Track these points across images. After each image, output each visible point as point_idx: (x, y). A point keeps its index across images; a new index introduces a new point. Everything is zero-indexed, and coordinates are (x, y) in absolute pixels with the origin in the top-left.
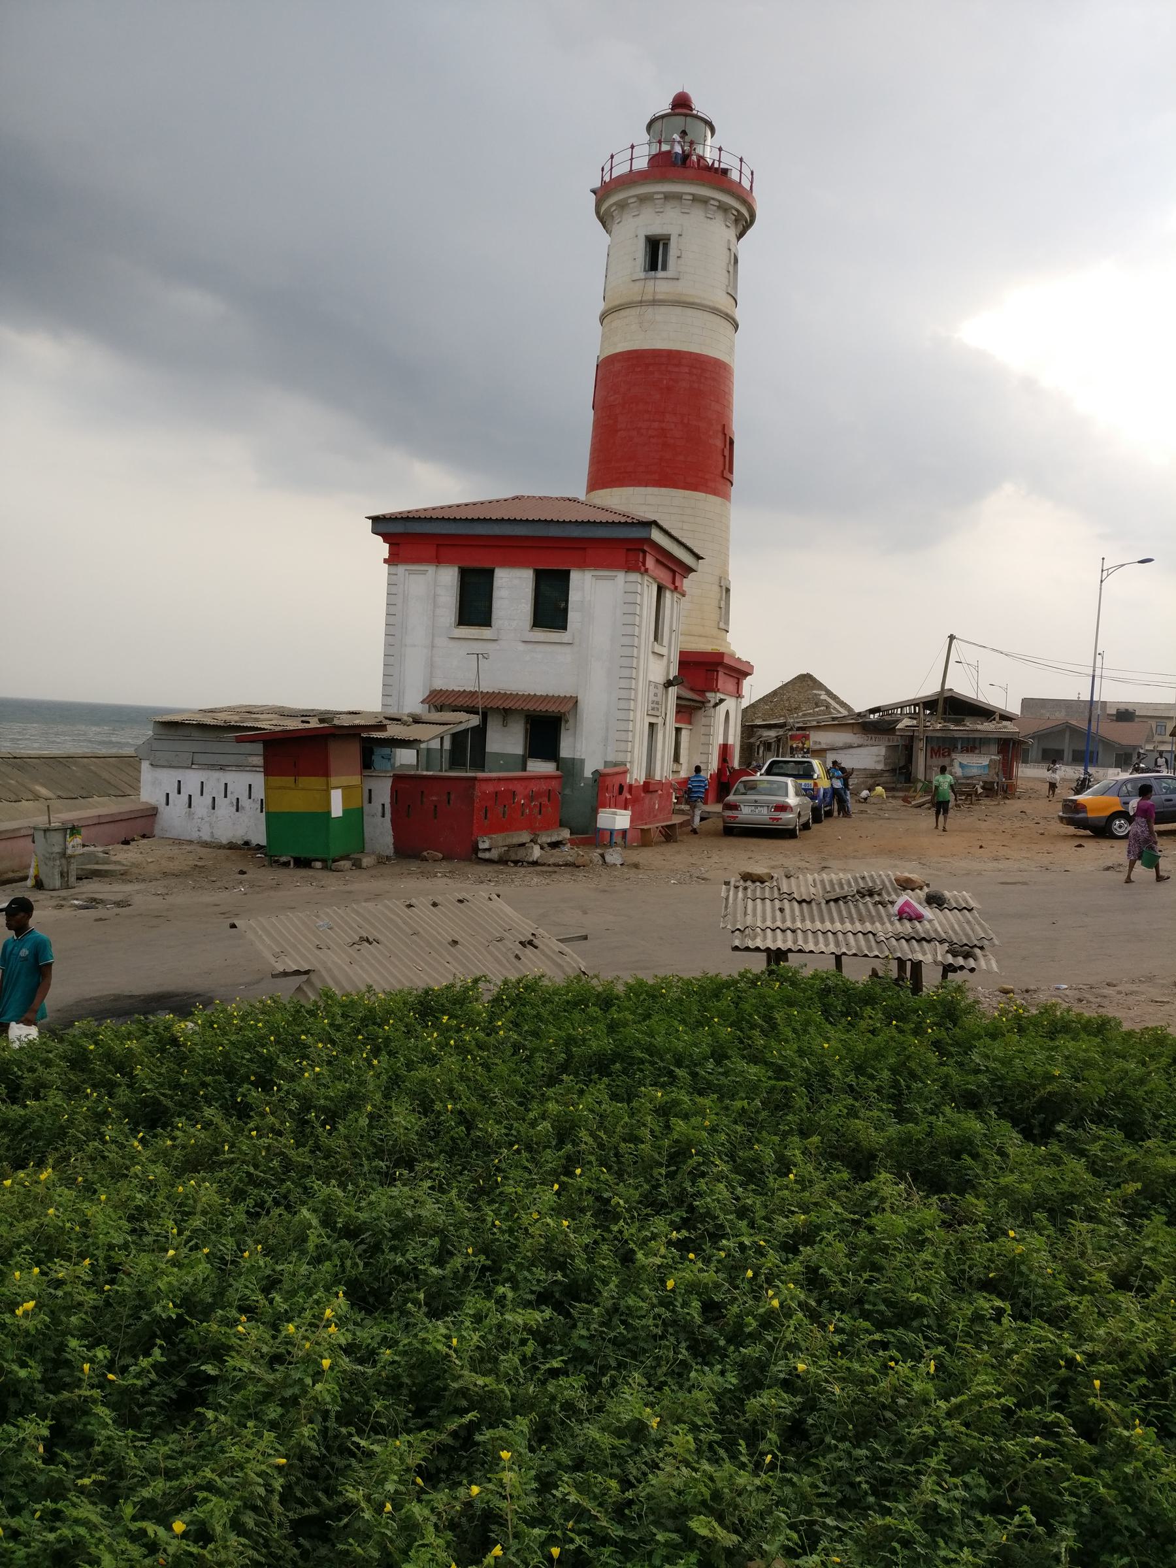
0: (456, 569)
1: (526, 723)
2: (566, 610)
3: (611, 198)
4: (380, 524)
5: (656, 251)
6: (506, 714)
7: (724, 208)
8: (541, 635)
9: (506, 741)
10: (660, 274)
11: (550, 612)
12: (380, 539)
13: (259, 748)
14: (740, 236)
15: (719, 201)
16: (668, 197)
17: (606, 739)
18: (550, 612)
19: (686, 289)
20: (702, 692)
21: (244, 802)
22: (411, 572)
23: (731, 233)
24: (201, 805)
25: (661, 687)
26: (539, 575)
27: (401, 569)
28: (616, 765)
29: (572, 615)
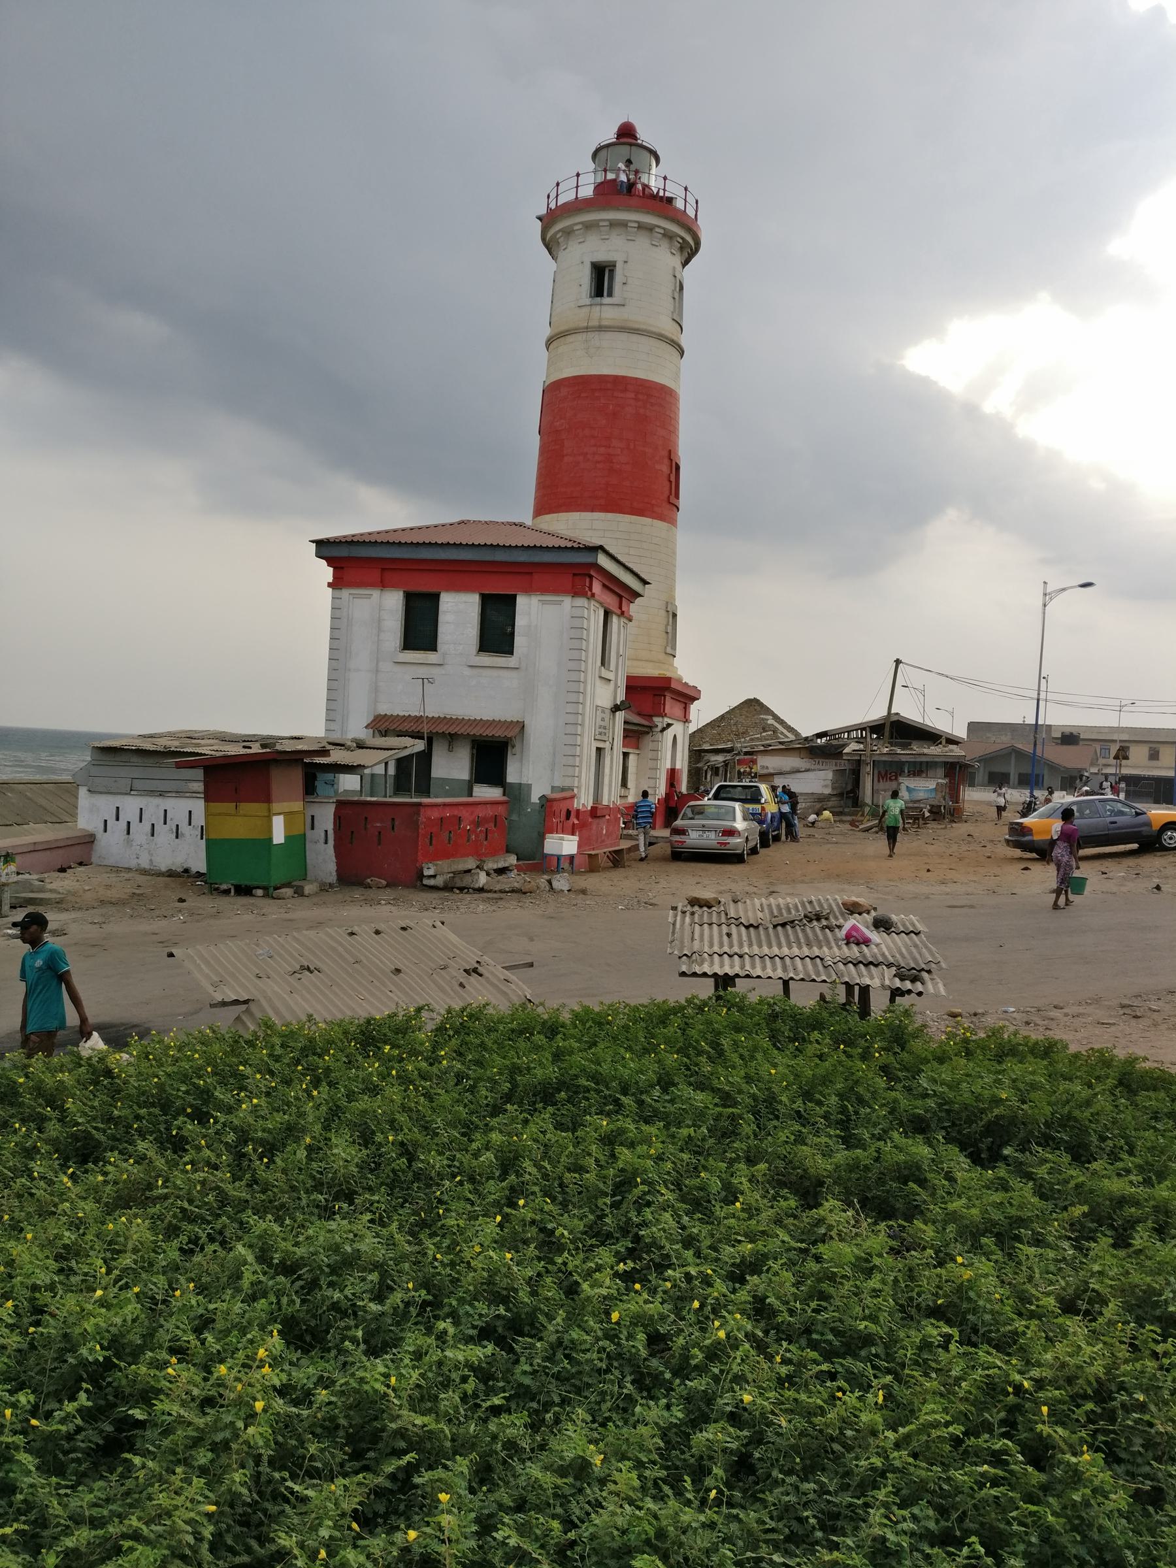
0: (401, 593)
1: (473, 748)
2: (512, 634)
3: (556, 225)
4: (325, 548)
5: (602, 278)
6: (452, 739)
7: (669, 236)
8: (487, 659)
9: (453, 766)
10: (606, 300)
11: (496, 636)
12: (324, 562)
13: (199, 773)
14: (685, 263)
15: (581, 223)
16: (613, 224)
17: (553, 764)
18: (496, 636)
19: (632, 315)
20: (650, 717)
21: (184, 828)
22: (355, 597)
23: (677, 261)
24: (140, 832)
25: (608, 712)
26: (487, 601)
27: (345, 593)
28: (563, 790)
29: (518, 640)
